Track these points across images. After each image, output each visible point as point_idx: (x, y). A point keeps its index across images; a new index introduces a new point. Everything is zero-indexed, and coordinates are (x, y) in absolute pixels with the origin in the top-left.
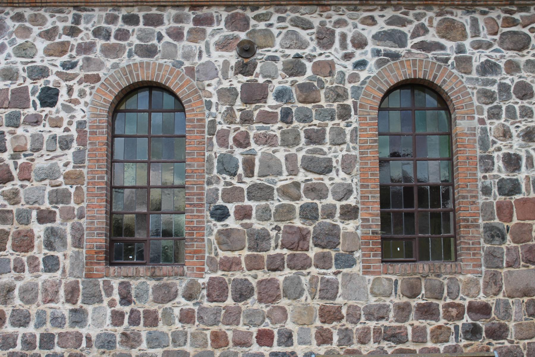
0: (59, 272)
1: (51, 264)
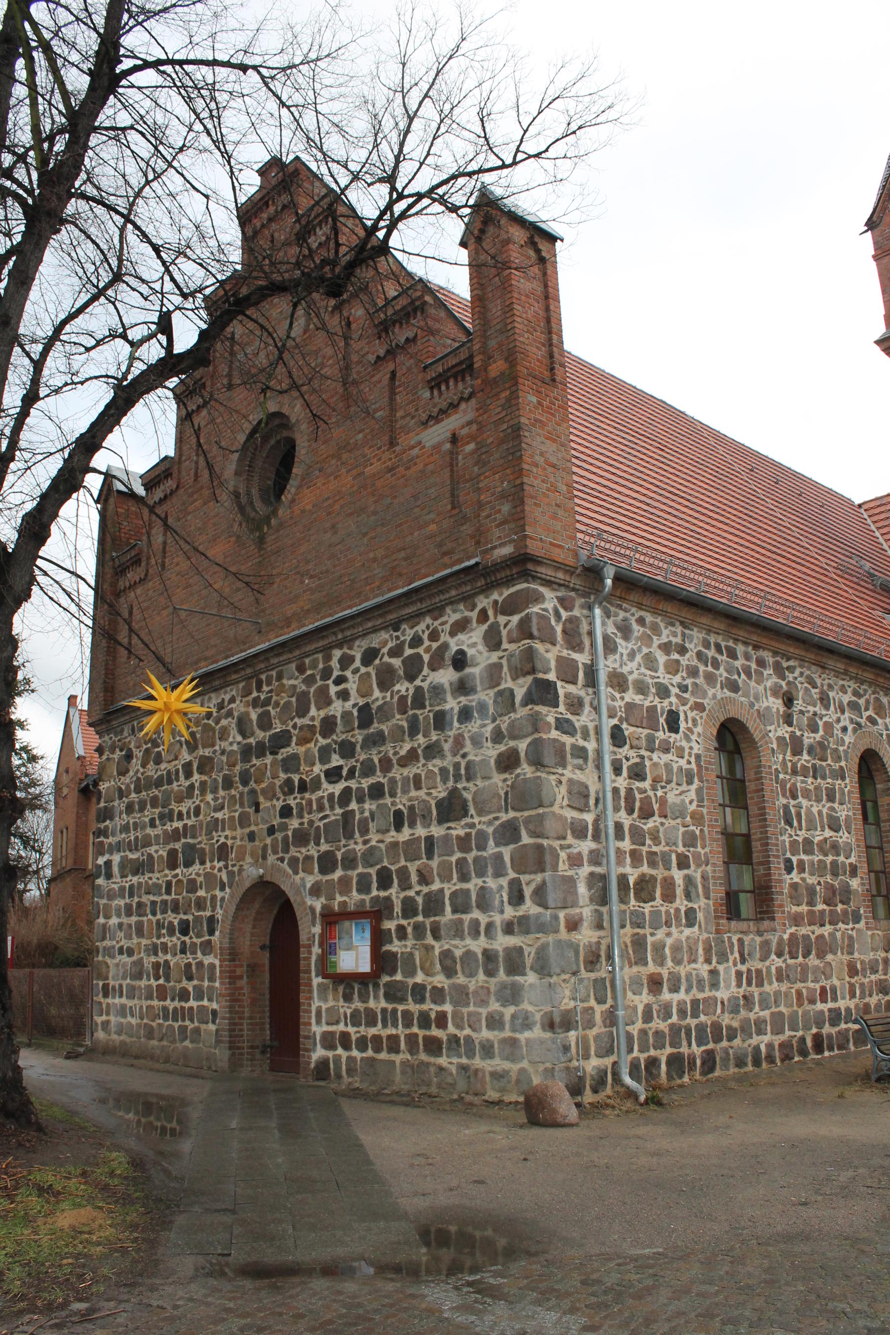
0: (697, 927)
1: (691, 916)
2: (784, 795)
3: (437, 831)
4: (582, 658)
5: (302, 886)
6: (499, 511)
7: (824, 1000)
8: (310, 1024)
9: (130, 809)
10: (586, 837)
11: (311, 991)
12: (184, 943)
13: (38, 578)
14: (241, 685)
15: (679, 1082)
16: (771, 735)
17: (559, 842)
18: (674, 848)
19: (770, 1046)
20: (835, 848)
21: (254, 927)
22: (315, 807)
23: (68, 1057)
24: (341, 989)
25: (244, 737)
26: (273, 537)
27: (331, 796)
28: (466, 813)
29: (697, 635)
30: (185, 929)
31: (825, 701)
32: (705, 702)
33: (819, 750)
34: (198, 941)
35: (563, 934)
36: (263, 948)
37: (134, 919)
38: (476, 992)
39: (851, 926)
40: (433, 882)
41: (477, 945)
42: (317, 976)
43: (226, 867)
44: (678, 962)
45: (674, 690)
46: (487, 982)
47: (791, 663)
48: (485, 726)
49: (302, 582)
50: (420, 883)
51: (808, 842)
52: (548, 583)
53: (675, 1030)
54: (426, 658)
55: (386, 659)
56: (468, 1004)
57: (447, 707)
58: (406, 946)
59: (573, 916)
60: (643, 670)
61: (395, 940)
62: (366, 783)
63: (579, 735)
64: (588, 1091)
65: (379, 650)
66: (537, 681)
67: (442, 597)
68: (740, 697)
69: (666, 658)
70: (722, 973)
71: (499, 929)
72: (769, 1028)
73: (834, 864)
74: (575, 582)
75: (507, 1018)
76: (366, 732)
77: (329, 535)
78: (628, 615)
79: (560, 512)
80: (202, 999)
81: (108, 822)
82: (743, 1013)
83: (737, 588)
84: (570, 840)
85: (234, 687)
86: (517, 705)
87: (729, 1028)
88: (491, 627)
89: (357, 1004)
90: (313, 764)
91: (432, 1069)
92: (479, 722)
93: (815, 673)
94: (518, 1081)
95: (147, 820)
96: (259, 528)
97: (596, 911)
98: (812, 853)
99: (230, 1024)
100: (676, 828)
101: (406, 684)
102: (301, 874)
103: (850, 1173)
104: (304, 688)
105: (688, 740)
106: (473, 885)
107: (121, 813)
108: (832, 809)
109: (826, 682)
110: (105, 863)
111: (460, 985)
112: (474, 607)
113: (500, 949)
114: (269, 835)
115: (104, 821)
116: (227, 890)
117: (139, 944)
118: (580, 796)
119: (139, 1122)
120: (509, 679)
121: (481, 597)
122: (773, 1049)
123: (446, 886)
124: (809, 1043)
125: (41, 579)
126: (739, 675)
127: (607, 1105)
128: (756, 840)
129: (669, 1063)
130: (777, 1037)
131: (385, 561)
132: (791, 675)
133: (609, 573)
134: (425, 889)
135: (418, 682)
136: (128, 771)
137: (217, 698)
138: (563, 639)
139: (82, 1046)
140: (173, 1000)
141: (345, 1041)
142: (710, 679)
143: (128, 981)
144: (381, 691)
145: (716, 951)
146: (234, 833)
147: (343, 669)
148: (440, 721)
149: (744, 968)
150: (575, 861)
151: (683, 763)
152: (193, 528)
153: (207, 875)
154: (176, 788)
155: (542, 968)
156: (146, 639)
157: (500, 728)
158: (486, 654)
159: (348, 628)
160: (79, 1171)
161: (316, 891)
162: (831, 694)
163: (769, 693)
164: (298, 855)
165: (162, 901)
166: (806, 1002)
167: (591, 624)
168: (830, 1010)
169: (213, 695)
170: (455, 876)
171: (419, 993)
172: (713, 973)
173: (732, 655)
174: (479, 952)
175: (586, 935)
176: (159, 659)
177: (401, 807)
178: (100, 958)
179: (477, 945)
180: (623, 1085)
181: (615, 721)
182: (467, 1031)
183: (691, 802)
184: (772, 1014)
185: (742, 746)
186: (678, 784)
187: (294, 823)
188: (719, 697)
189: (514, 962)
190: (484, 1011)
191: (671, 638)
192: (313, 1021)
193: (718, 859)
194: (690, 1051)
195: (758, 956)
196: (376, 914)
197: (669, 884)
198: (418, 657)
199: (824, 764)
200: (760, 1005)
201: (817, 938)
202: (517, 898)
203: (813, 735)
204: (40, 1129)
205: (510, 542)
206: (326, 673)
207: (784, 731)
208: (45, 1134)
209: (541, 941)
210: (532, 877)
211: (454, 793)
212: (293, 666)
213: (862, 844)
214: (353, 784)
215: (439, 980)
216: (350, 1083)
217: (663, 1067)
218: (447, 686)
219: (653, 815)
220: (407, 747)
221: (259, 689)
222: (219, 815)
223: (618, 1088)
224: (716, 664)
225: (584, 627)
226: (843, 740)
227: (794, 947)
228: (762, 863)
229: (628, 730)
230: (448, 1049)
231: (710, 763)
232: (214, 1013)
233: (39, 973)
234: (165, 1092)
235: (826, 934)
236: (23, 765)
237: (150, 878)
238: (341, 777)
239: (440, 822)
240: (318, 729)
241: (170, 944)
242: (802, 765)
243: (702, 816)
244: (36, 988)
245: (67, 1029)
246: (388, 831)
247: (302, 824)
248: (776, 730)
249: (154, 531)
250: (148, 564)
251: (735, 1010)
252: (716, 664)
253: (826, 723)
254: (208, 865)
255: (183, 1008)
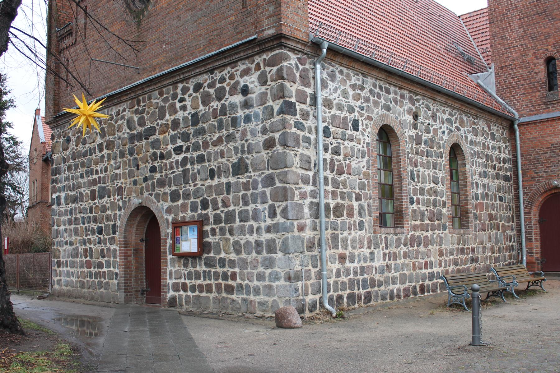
0: (364, 230)
1: (361, 226)
2: (411, 165)
3: (232, 180)
4: (309, 91)
5: (162, 209)
6: (268, 10)
7: (426, 268)
8: (166, 279)
9: (69, 168)
10: (309, 183)
11: (166, 262)
12: (100, 238)
13: (11, 39)
14: (129, 102)
15: (353, 307)
16: (406, 134)
17: (295, 186)
18: (354, 190)
19: (399, 290)
20: (436, 193)
21: (137, 230)
22: (168, 167)
23: (39, 299)
24: (182, 261)
25: (131, 130)
26: (146, 22)
27: (177, 161)
28: (247, 171)
29: (370, 81)
30: (100, 231)
31: (434, 117)
32: (373, 116)
33: (430, 143)
34: (107, 237)
35: (296, 233)
36: (142, 240)
37: (73, 226)
38: (251, 262)
39: (441, 232)
40: (230, 206)
41: (252, 239)
42: (170, 254)
43: (122, 199)
44: (354, 248)
45: (357, 109)
46: (257, 257)
47: (418, 97)
48: (258, 125)
49: (161, 47)
50: (223, 206)
51: (422, 189)
52: (293, 50)
53: (352, 282)
54: (227, 89)
55: (206, 89)
56: (247, 268)
57: (238, 115)
58: (215, 239)
59: (301, 224)
60: (341, 98)
61: (210, 236)
62: (195, 154)
63: (307, 131)
64: (307, 311)
65: (203, 84)
66: (285, 102)
67: (237, 56)
68: (390, 114)
69: (354, 92)
70: (376, 254)
71: (263, 230)
72: (398, 281)
73: (435, 200)
74: (307, 50)
75: (267, 275)
76: (195, 128)
77: (176, 21)
78: (334, 68)
79: (301, 12)
80: (110, 267)
81: (58, 175)
82: (386, 274)
83: (392, 57)
84: (301, 185)
85: (125, 103)
86: (275, 114)
87: (379, 281)
88: (262, 73)
89: (191, 269)
90: (168, 144)
91: (229, 301)
92: (255, 123)
93: (430, 103)
94: (272, 306)
95: (79, 174)
96: (138, 17)
97: (313, 221)
98: (424, 195)
99: (125, 280)
100: (354, 181)
101: (217, 103)
102: (161, 202)
103: (434, 349)
104: (162, 104)
105: (363, 135)
106: (250, 208)
107: (65, 171)
108: (435, 173)
109: (436, 107)
110: (57, 197)
111: (243, 258)
112: (253, 61)
113: (264, 240)
114: (144, 182)
115: (56, 175)
116: (123, 210)
117: (76, 239)
118: (306, 163)
119: (78, 330)
120: (271, 100)
121: (257, 57)
122: (400, 292)
123: (236, 208)
124: (418, 289)
125: (13, 39)
126: (391, 102)
127: (316, 318)
128: (396, 188)
129: (348, 298)
130: (402, 286)
131: (206, 36)
132: (418, 104)
133: (326, 45)
134: (226, 210)
135: (223, 102)
136: (68, 148)
137: (116, 109)
138: (300, 80)
139: (47, 293)
140: (94, 268)
141: (184, 287)
142: (376, 104)
143: (71, 258)
144: (204, 106)
145: (373, 243)
146: (126, 181)
147: (183, 94)
148: (234, 122)
149: (387, 251)
150: (303, 196)
151: (360, 147)
152: (101, 16)
153: (112, 203)
154: (95, 157)
155: (285, 250)
156: (76, 77)
157: (265, 126)
158: (259, 87)
159: (186, 72)
160: (44, 353)
161: (169, 211)
162: (438, 114)
163: (406, 112)
164: (160, 192)
165: (88, 217)
166: (417, 269)
167: (315, 73)
168: (429, 273)
169: (113, 107)
170: (241, 203)
171: (222, 262)
172: (372, 253)
173: (388, 92)
174: (253, 242)
175: (308, 233)
176: (83, 86)
177: (213, 167)
178: (55, 247)
179: (252, 239)
180: (325, 308)
181: (326, 124)
182: (247, 282)
183: (363, 167)
184: (400, 274)
185: (391, 139)
186: (357, 158)
187: (158, 176)
188: (380, 114)
189: (271, 248)
190: (255, 272)
191: (356, 82)
192: (168, 277)
193: (376, 197)
194: (359, 292)
195: (395, 245)
196: (201, 223)
197: (351, 208)
198: (223, 88)
199: (432, 150)
200: (394, 270)
201: (424, 237)
202: (273, 214)
203: (427, 135)
204: (22, 333)
205: (273, 27)
206: (175, 96)
207: (413, 132)
208: (26, 336)
209: (285, 236)
210: (281, 203)
211: (241, 160)
212: (157, 92)
213: (449, 191)
214: (188, 155)
215: (233, 256)
216: (187, 309)
217: (345, 300)
218: (238, 104)
219: (344, 173)
220: (217, 135)
221: (138, 104)
222: (118, 171)
223: (322, 310)
224: (379, 96)
225: (311, 74)
226: (442, 138)
227: (412, 241)
228: (398, 199)
229: (332, 129)
230: (237, 291)
231: (374, 147)
232: (116, 274)
233: (22, 256)
234: (91, 314)
235: (429, 235)
236: (11, 147)
237: (81, 205)
238: (182, 151)
239: (234, 175)
240: (170, 126)
241: (92, 239)
242: (421, 150)
243: (369, 174)
244: (21, 263)
245: (38, 284)
246: (207, 179)
247: (161, 176)
248: (408, 132)
249: (79, 17)
250: (76, 35)
251: (382, 272)
252: (379, 96)
253: (434, 129)
254: (112, 197)
255: (100, 272)
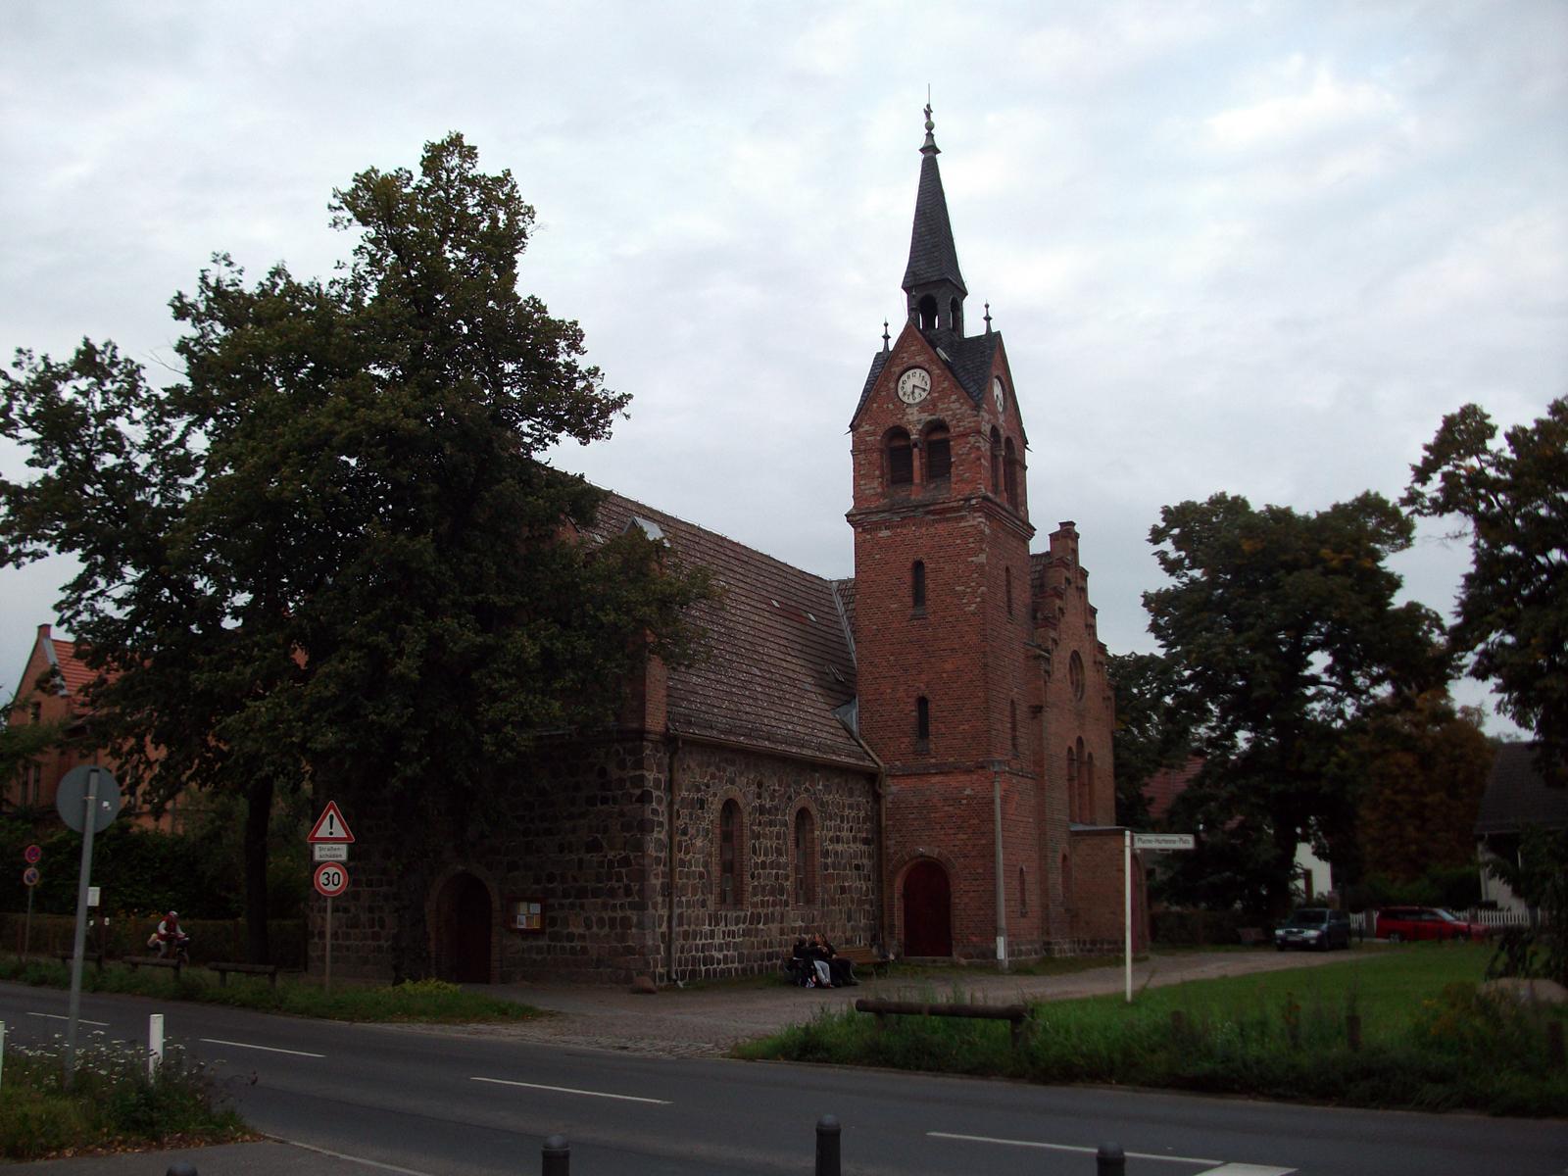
20: (779, 866)
171: (570, 937)
